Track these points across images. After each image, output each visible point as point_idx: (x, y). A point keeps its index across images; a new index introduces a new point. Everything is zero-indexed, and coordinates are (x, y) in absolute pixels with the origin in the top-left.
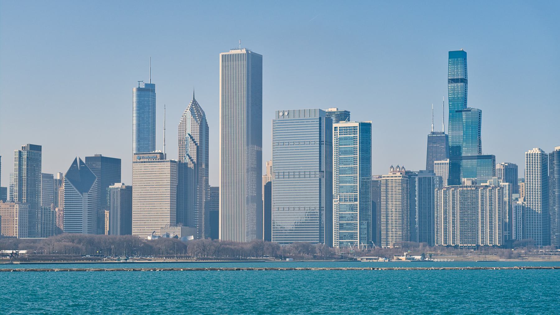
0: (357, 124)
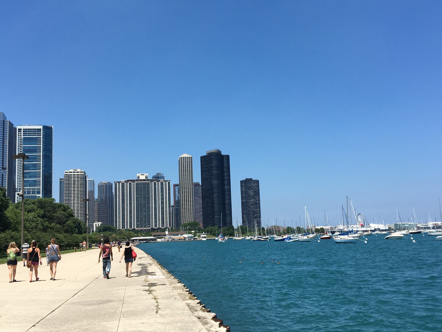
0: (41, 127)
